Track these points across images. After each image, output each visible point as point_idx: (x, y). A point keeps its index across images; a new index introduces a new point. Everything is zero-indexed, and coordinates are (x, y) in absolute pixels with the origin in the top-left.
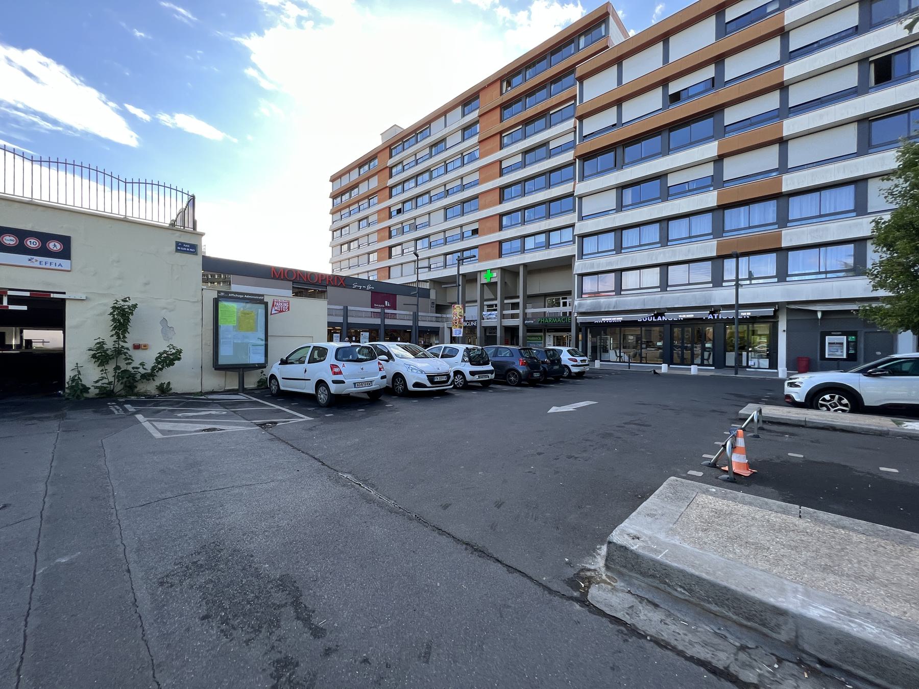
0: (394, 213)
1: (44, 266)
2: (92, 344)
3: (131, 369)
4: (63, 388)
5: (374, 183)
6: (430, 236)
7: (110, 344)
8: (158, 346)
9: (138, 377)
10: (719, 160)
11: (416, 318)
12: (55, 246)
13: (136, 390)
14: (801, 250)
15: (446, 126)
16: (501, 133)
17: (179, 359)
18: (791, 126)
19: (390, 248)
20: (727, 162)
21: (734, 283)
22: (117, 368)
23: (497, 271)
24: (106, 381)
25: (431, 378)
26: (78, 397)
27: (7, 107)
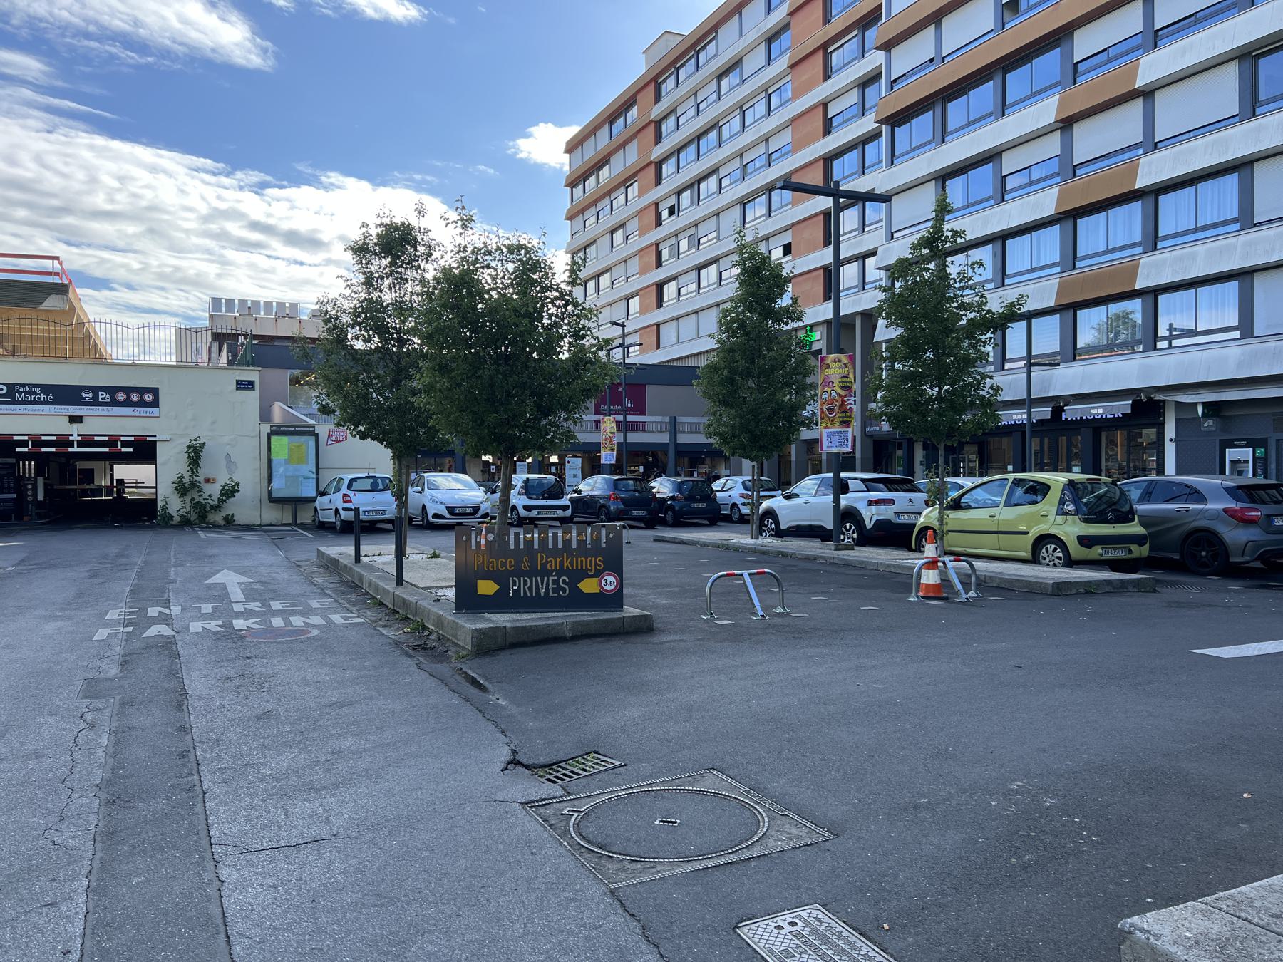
0: (665, 214)
1: (142, 415)
2: (175, 479)
3: (202, 500)
4: (156, 519)
5: (631, 157)
6: (719, 259)
7: (187, 479)
8: (223, 479)
9: (208, 508)
10: (1066, 124)
11: (674, 428)
12: (149, 397)
13: (207, 520)
14: (1187, 289)
15: (741, 35)
16: (824, 47)
17: (238, 491)
18: (1151, 68)
19: (660, 287)
20: (1079, 129)
21: (1022, 364)
22: (193, 499)
23: (820, 328)
24: (184, 510)
25: (451, 509)
26: (166, 523)
27: (74, 36)
